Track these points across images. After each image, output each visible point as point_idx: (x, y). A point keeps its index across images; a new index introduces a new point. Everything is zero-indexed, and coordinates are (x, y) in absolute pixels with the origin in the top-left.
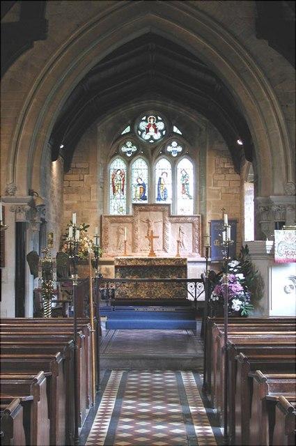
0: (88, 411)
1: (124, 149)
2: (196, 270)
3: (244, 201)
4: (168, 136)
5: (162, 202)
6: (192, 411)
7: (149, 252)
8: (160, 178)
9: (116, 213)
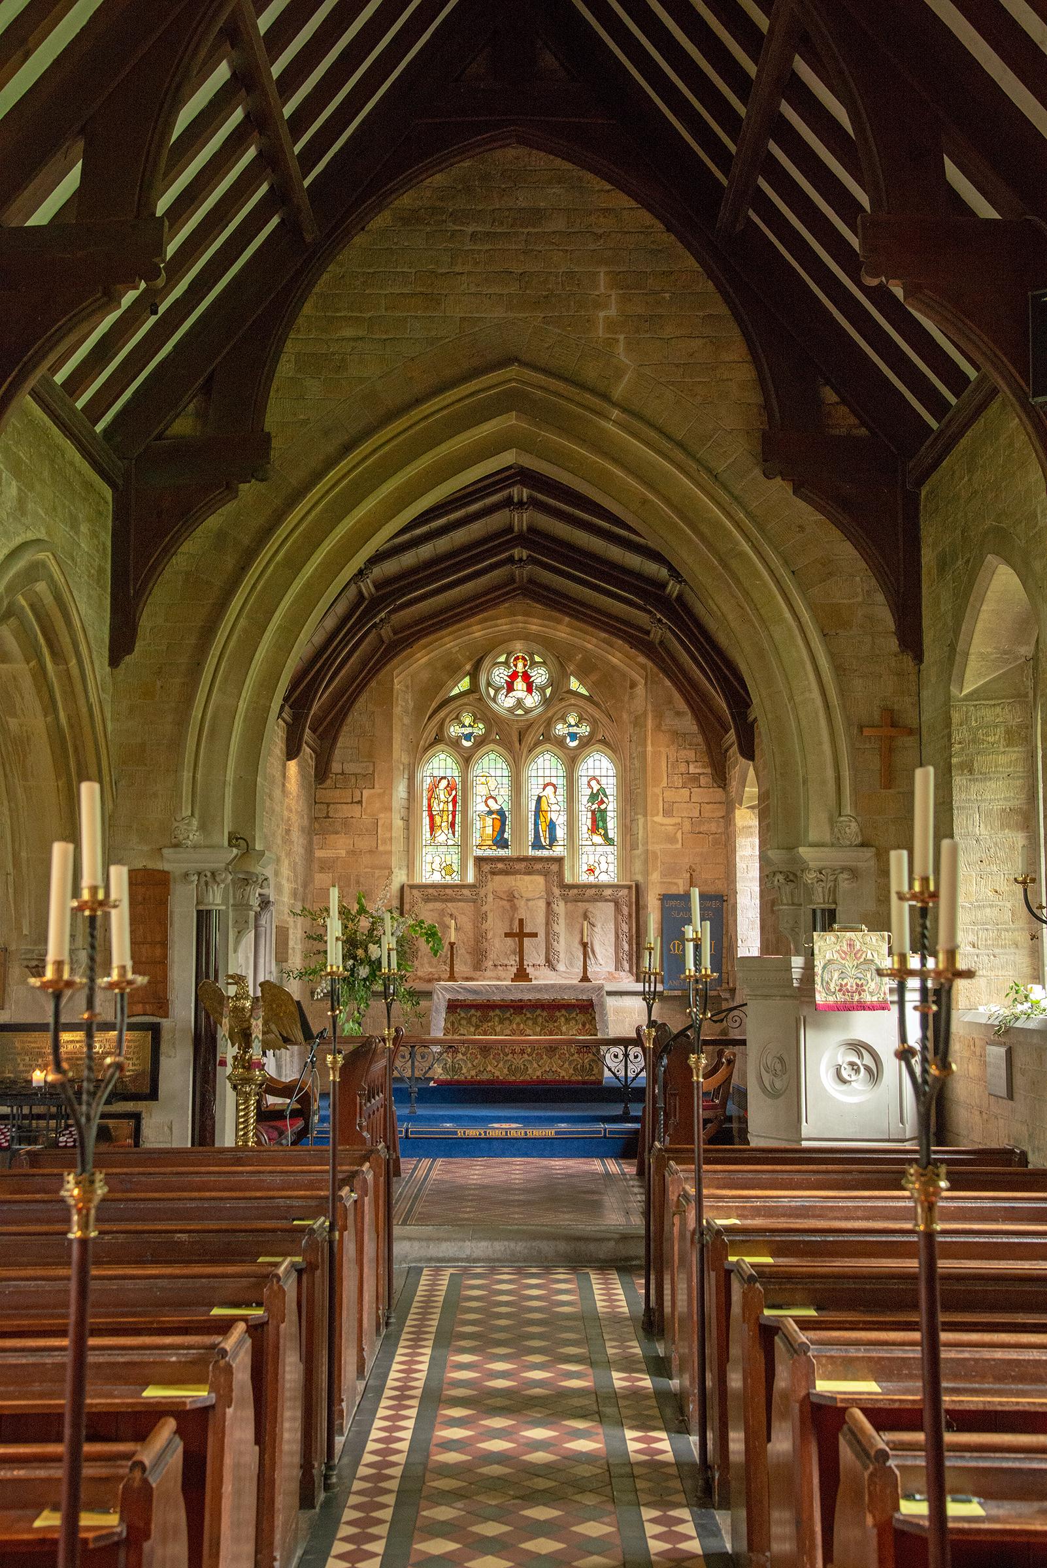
0: (360, 1386)
1: (454, 730)
2: (625, 1014)
3: (734, 851)
4: (557, 697)
5: (545, 853)
6: (618, 1384)
7: (514, 970)
8: (539, 798)
9: (436, 878)
